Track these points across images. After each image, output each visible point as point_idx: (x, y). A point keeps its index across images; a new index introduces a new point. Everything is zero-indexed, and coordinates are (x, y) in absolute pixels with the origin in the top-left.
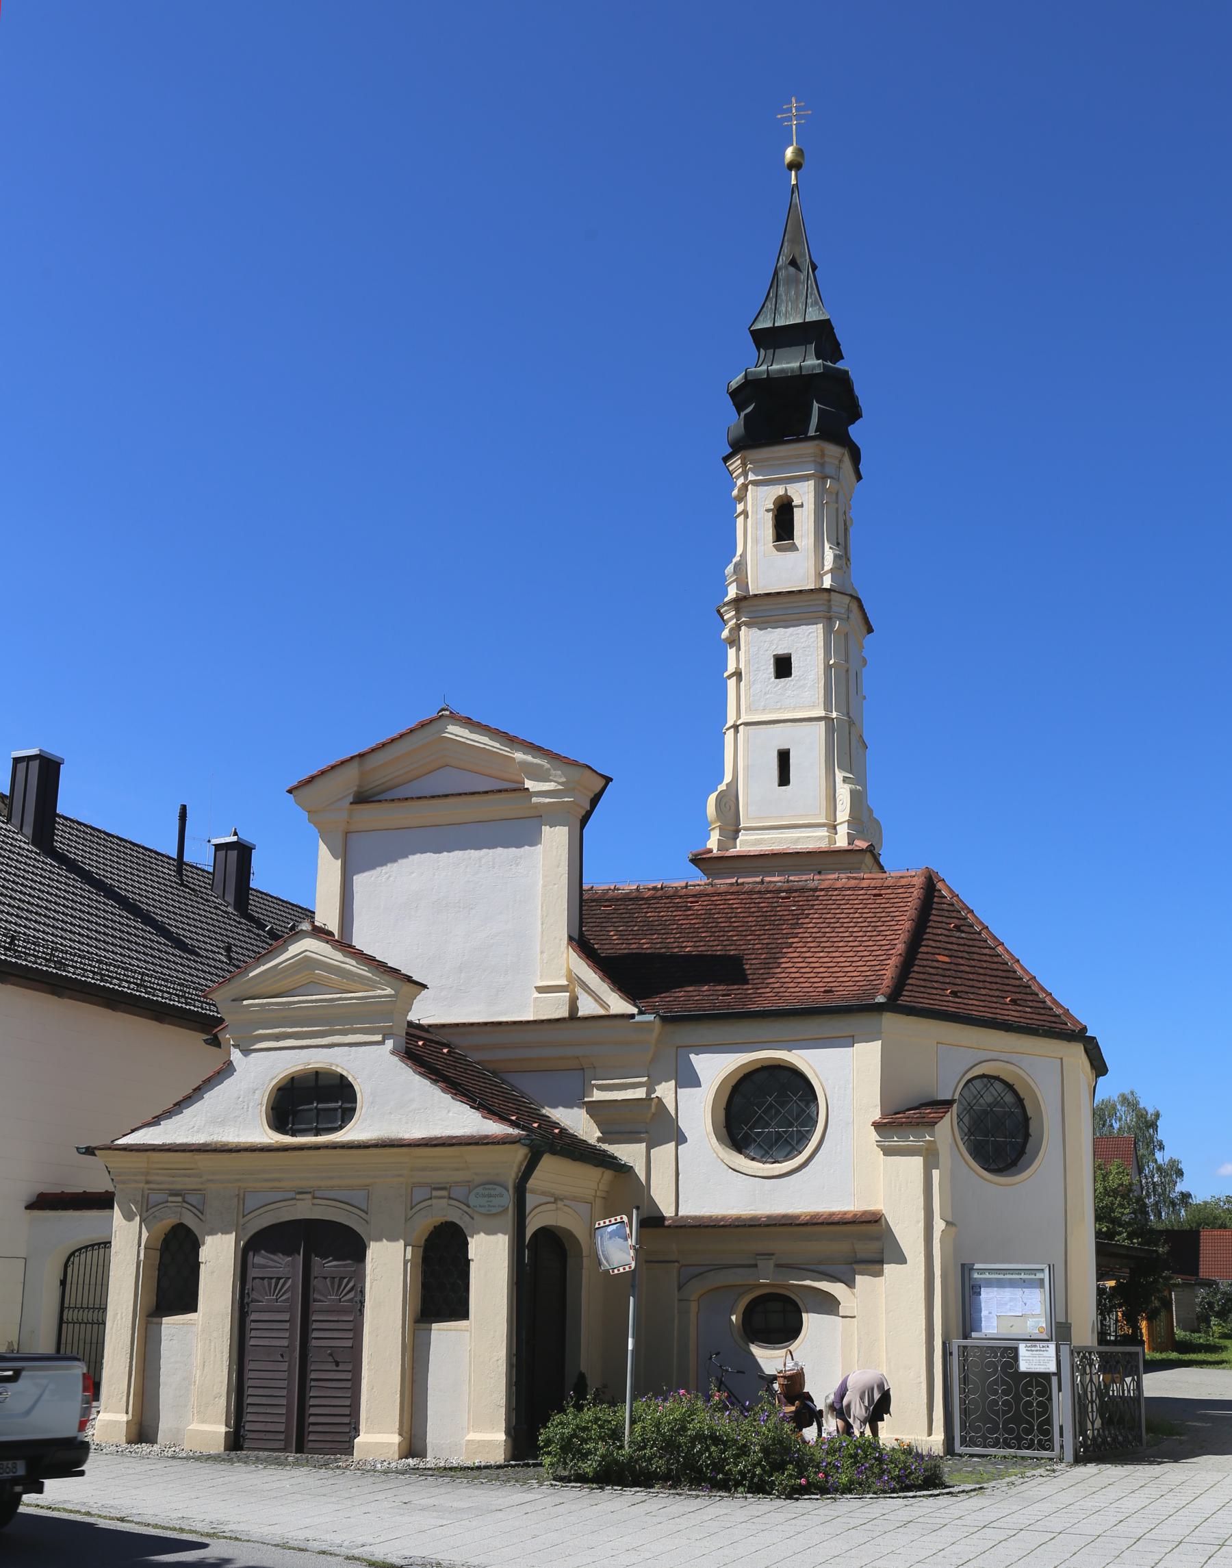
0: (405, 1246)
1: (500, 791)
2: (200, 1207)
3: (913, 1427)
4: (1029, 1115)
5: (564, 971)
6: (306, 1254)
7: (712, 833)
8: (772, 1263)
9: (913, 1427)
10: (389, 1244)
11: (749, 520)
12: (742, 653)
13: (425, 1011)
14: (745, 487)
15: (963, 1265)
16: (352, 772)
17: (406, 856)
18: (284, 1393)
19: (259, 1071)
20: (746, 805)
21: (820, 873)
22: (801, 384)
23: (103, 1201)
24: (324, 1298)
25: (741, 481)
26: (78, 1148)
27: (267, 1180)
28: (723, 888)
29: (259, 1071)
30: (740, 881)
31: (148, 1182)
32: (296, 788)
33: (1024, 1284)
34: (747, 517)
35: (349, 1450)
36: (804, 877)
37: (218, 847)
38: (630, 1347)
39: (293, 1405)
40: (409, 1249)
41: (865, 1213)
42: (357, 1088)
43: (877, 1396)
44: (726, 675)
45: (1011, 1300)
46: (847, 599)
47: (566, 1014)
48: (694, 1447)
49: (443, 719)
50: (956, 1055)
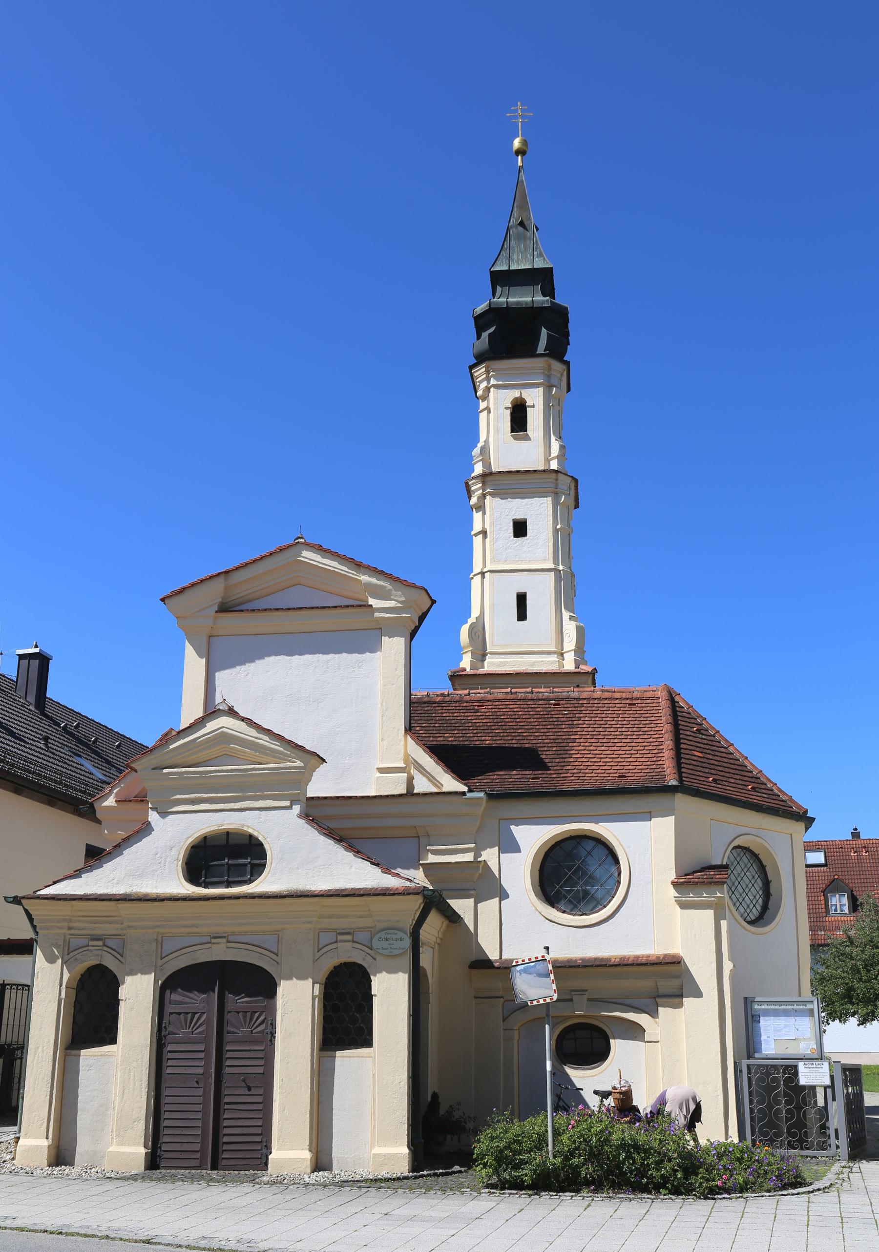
0: (313, 983)
1: (348, 606)
2: (121, 951)
3: (717, 1129)
4: (770, 879)
5: (402, 756)
6: (221, 992)
8: (585, 998)
9: (717, 1129)
10: (298, 982)
11: (491, 415)
12: (487, 517)
13: (321, 785)
14: (488, 389)
15: (746, 999)
16: (218, 585)
18: (200, 1116)
19: (174, 832)
21: (578, 686)
23: (24, 948)
24: (237, 1030)
26: (5, 898)
27: (185, 926)
28: (501, 696)
29: (174, 832)
31: (70, 928)
32: (168, 597)
33: (796, 1013)
34: (489, 412)
35: (264, 1165)
36: (566, 690)
37: (22, 657)
38: (549, 1068)
39: (208, 1126)
40: (317, 986)
41: (665, 956)
42: (266, 846)
43: (692, 1107)
44: (473, 533)
45: (786, 1026)
46: (570, 479)
47: (405, 792)
48: (620, 1154)
49: (299, 546)
50: (726, 827)
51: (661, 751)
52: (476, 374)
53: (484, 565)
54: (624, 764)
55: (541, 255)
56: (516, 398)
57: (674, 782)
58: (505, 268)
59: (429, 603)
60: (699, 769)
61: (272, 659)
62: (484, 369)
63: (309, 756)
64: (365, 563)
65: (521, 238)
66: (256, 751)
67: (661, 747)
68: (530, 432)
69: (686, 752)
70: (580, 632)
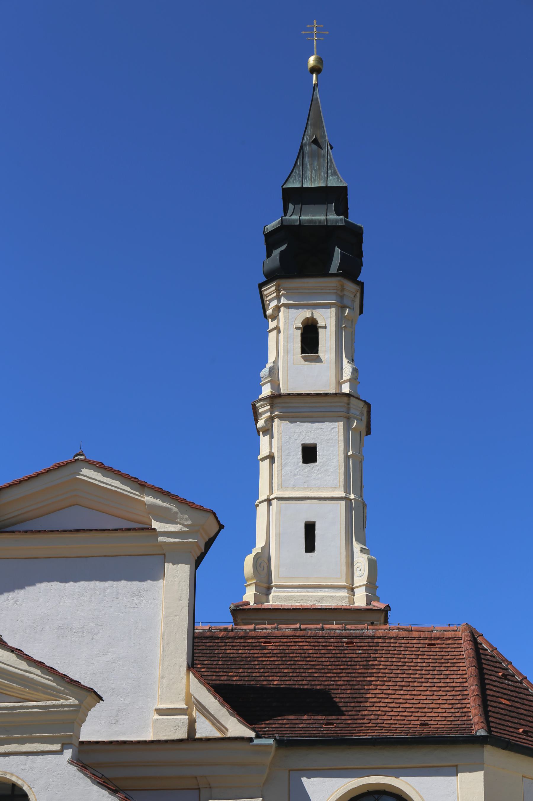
1: (129, 529)
5: (183, 695)
7: (248, 589)
11: (281, 335)
12: (275, 441)
14: (277, 309)
17: (32, 584)
20: (278, 566)
21: (372, 624)
22: (326, 235)
25: (274, 303)
28: (288, 632)
30: (303, 627)
34: (279, 332)
36: (360, 627)
44: (259, 457)
46: (361, 404)
47: (185, 736)
51: (465, 697)
52: (265, 293)
53: (271, 492)
54: (426, 710)
55: (335, 174)
56: (307, 319)
57: (482, 733)
58: (298, 185)
59: (217, 528)
60: (507, 718)
61: (43, 588)
62: (274, 288)
63: (84, 693)
64: (150, 482)
65: (315, 156)
66: (25, 686)
67: (466, 693)
68: (321, 353)
69: (494, 699)
70: (372, 566)
